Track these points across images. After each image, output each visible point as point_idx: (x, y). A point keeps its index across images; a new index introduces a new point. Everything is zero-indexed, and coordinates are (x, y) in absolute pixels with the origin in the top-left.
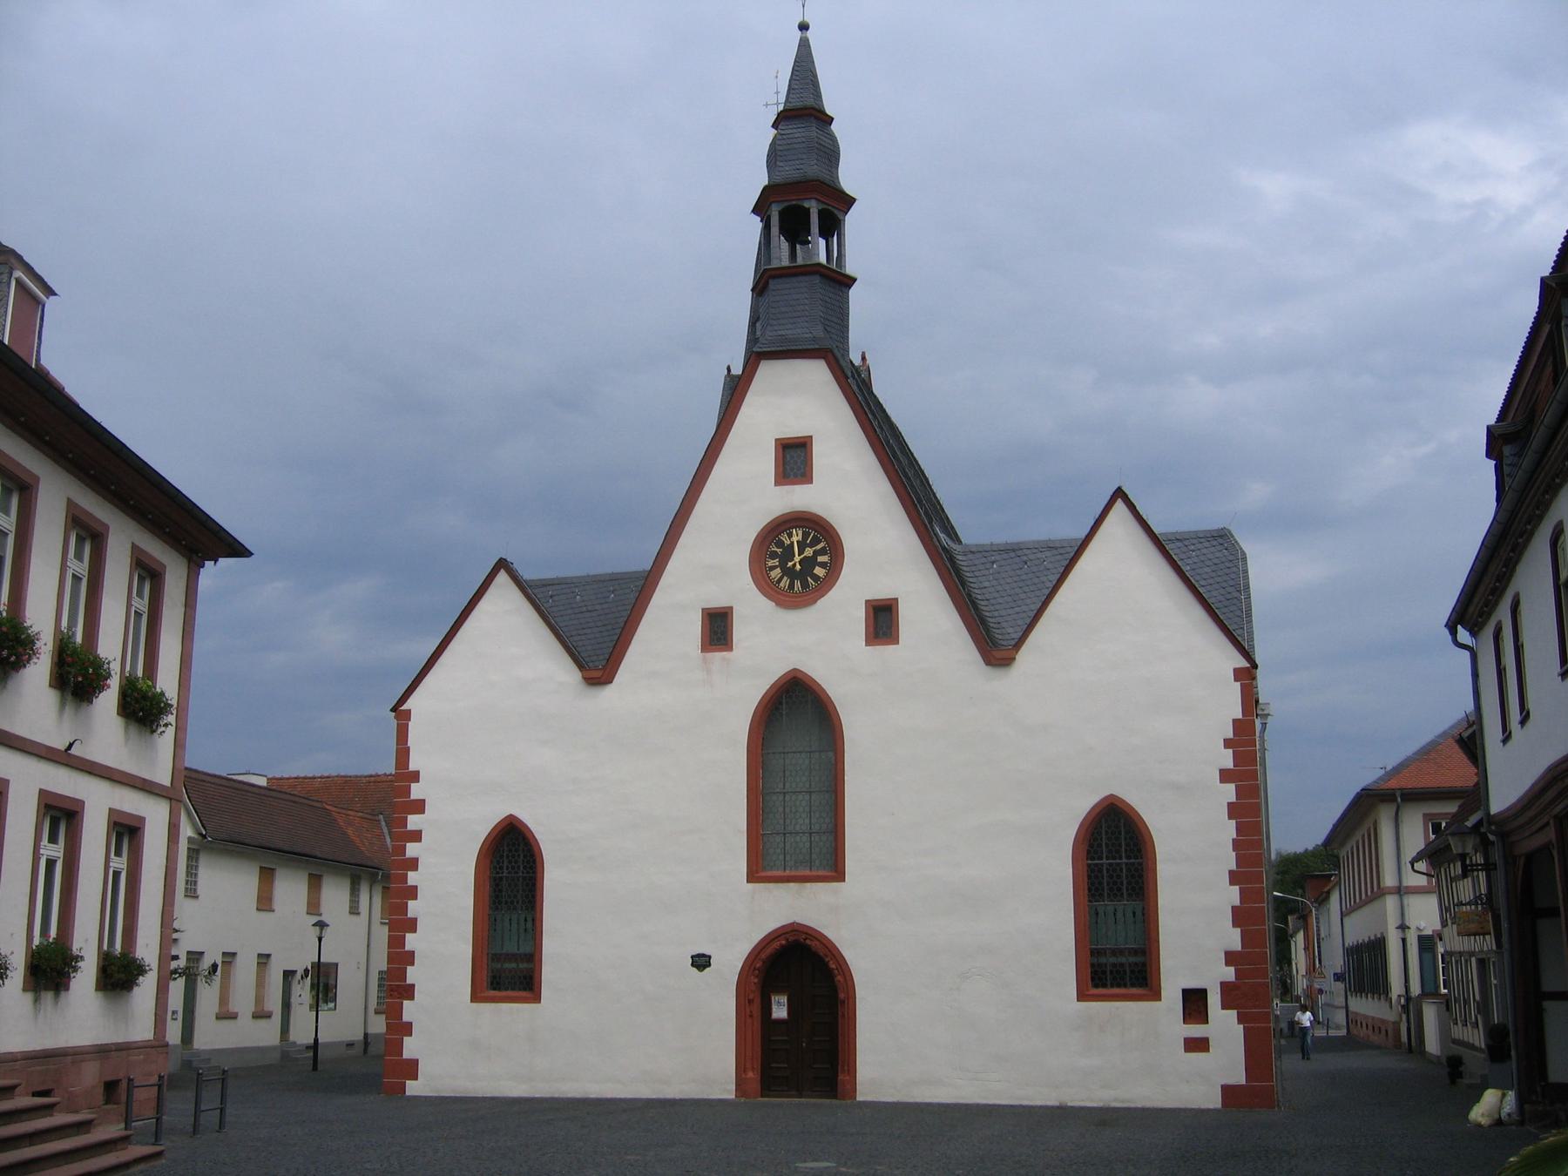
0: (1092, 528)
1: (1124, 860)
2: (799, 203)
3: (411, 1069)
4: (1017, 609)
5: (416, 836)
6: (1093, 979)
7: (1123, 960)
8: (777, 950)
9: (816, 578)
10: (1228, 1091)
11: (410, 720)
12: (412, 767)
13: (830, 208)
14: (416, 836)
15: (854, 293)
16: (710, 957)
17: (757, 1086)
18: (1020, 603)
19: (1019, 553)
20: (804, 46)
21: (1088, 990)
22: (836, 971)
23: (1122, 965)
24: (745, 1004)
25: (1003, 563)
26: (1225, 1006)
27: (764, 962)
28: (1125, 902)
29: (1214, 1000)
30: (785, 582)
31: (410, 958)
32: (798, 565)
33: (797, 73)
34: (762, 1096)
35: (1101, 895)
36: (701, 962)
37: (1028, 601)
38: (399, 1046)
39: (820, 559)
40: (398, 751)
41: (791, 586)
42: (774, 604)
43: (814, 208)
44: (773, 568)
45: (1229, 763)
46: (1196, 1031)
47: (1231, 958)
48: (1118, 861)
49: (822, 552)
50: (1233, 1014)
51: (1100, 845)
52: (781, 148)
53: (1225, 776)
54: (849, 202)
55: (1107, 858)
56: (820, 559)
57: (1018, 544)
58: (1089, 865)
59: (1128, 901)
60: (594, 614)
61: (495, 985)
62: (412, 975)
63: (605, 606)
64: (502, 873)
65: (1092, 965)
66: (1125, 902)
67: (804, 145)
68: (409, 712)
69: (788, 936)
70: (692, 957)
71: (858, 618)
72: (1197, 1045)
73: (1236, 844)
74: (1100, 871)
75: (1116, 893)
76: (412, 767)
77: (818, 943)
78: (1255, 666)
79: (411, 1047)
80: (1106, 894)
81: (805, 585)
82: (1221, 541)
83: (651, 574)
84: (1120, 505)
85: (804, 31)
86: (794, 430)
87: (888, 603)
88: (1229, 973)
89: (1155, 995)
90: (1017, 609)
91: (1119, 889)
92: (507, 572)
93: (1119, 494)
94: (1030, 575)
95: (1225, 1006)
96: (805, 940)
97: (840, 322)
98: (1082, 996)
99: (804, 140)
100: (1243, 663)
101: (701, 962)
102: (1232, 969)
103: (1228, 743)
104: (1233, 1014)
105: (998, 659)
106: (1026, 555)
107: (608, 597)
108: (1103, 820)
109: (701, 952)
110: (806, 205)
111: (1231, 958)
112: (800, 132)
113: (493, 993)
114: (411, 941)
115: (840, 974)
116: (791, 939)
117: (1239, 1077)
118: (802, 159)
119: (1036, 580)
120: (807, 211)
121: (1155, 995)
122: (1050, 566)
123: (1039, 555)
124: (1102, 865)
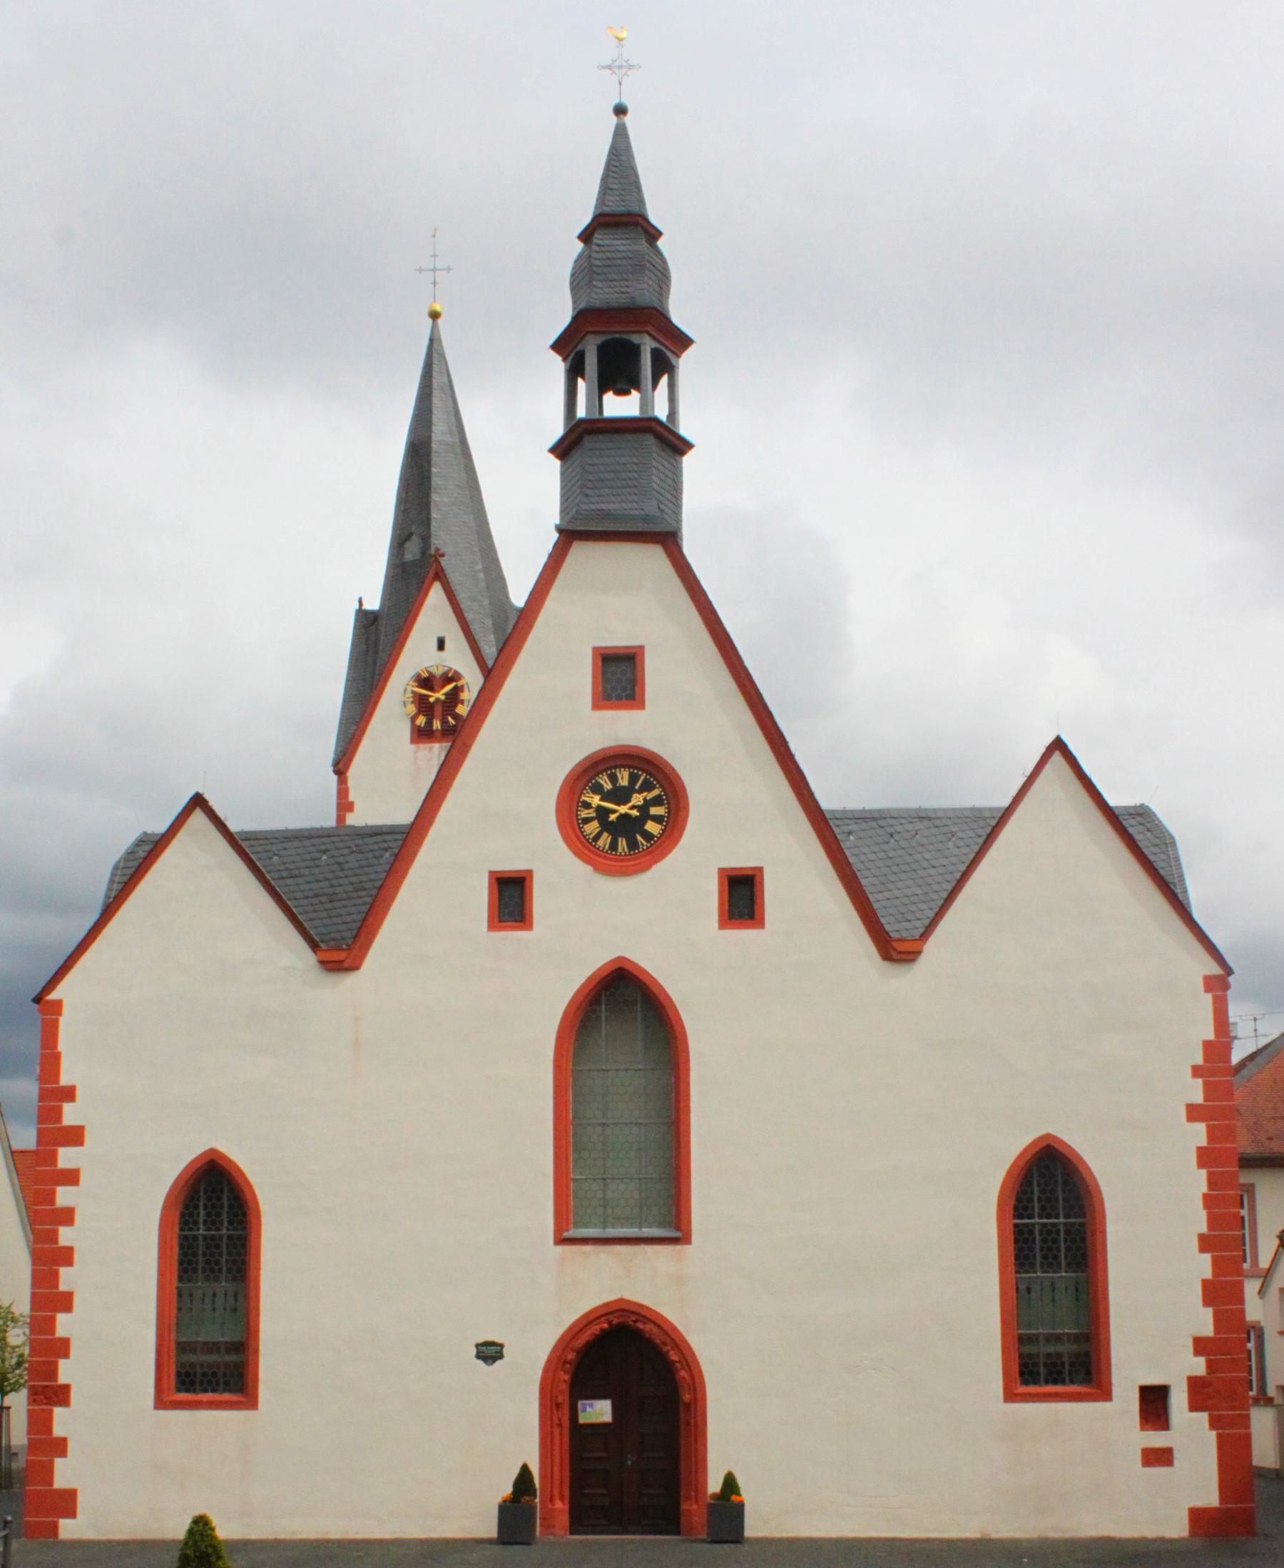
0: (90, 931)
1: (1061, 1220)
2: (625, 336)
3: (66, 1503)
4: (887, 894)
5: (71, 1177)
6: (1021, 1374)
7: (1060, 1348)
8: (596, 1335)
9: (648, 836)
10: (1197, 1516)
11: (60, 1014)
12: (65, 1080)
13: (663, 349)
14: (71, 1177)
15: (687, 460)
16: (502, 1346)
17: (564, 1519)
18: (891, 886)
19: (882, 823)
20: (621, 134)
21: (1016, 1388)
22: (678, 1365)
23: (1059, 1355)
24: (552, 1406)
25: (862, 834)
26: (1194, 1407)
27: (578, 1353)
28: (1064, 1274)
29: (1179, 1400)
30: (605, 840)
31: (63, 1348)
32: (617, 815)
33: (613, 169)
34: (571, 1533)
35: (1032, 1265)
36: (490, 1352)
37: (900, 885)
38: (48, 1471)
39: (654, 811)
40: (43, 1057)
41: (614, 846)
42: (592, 868)
43: (647, 346)
44: (587, 821)
45: (1198, 1098)
46: (1157, 1439)
47: (1200, 1346)
48: (1055, 1221)
49: (657, 801)
50: (1204, 1416)
51: (1031, 1200)
52: (598, 263)
53: (1194, 1113)
54: (684, 342)
55: (1040, 1217)
56: (654, 811)
57: (879, 811)
58: (1016, 1226)
59: (1066, 1272)
60: (300, 880)
61: (205, 1385)
62: (66, 1372)
63: (316, 871)
64: (198, 1230)
65: (1021, 1356)
66: (1064, 1274)
67: (630, 262)
68: (58, 1004)
69: (611, 1317)
70: (477, 1346)
71: (710, 895)
72: (1158, 1457)
73: (1209, 1201)
74: (1031, 1232)
75: (1051, 1263)
76: (65, 1080)
77: (655, 1329)
78: (1229, 971)
79: (64, 1474)
80: (1038, 1263)
81: (633, 845)
82: (1140, 819)
83: (414, 827)
84: (1057, 758)
85: (622, 116)
86: (619, 639)
87: (750, 873)
88: (1199, 1366)
89: (1104, 1392)
90: (887, 894)
91: (1056, 1257)
92: (204, 811)
93: (1058, 745)
94: (901, 852)
95: (1194, 1407)
96: (635, 1322)
97: (673, 500)
98: (1011, 1396)
99: (630, 255)
100: (1215, 970)
101: (490, 1352)
102: (1201, 1361)
103: (1197, 1071)
104: (1204, 1416)
105: (900, 953)
106: (892, 826)
107: (319, 859)
108: (1035, 1168)
109: (490, 1338)
110: (635, 339)
111: (1200, 1346)
112: (618, 244)
113: (183, 1396)
114: (64, 1324)
115: (683, 1368)
116: (615, 1321)
117: (1210, 1497)
118: (627, 280)
119: (909, 859)
120: (635, 350)
121: (1104, 1392)
122: (924, 841)
123: (909, 827)
124: (1033, 1225)
